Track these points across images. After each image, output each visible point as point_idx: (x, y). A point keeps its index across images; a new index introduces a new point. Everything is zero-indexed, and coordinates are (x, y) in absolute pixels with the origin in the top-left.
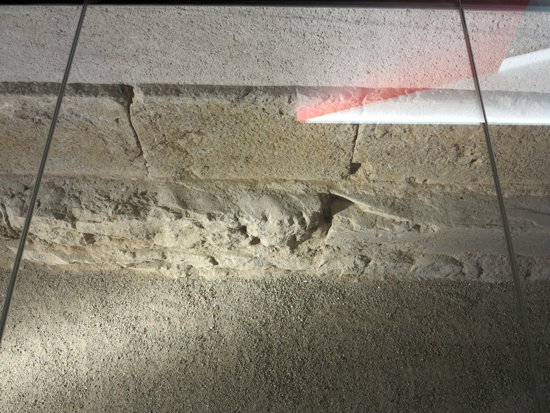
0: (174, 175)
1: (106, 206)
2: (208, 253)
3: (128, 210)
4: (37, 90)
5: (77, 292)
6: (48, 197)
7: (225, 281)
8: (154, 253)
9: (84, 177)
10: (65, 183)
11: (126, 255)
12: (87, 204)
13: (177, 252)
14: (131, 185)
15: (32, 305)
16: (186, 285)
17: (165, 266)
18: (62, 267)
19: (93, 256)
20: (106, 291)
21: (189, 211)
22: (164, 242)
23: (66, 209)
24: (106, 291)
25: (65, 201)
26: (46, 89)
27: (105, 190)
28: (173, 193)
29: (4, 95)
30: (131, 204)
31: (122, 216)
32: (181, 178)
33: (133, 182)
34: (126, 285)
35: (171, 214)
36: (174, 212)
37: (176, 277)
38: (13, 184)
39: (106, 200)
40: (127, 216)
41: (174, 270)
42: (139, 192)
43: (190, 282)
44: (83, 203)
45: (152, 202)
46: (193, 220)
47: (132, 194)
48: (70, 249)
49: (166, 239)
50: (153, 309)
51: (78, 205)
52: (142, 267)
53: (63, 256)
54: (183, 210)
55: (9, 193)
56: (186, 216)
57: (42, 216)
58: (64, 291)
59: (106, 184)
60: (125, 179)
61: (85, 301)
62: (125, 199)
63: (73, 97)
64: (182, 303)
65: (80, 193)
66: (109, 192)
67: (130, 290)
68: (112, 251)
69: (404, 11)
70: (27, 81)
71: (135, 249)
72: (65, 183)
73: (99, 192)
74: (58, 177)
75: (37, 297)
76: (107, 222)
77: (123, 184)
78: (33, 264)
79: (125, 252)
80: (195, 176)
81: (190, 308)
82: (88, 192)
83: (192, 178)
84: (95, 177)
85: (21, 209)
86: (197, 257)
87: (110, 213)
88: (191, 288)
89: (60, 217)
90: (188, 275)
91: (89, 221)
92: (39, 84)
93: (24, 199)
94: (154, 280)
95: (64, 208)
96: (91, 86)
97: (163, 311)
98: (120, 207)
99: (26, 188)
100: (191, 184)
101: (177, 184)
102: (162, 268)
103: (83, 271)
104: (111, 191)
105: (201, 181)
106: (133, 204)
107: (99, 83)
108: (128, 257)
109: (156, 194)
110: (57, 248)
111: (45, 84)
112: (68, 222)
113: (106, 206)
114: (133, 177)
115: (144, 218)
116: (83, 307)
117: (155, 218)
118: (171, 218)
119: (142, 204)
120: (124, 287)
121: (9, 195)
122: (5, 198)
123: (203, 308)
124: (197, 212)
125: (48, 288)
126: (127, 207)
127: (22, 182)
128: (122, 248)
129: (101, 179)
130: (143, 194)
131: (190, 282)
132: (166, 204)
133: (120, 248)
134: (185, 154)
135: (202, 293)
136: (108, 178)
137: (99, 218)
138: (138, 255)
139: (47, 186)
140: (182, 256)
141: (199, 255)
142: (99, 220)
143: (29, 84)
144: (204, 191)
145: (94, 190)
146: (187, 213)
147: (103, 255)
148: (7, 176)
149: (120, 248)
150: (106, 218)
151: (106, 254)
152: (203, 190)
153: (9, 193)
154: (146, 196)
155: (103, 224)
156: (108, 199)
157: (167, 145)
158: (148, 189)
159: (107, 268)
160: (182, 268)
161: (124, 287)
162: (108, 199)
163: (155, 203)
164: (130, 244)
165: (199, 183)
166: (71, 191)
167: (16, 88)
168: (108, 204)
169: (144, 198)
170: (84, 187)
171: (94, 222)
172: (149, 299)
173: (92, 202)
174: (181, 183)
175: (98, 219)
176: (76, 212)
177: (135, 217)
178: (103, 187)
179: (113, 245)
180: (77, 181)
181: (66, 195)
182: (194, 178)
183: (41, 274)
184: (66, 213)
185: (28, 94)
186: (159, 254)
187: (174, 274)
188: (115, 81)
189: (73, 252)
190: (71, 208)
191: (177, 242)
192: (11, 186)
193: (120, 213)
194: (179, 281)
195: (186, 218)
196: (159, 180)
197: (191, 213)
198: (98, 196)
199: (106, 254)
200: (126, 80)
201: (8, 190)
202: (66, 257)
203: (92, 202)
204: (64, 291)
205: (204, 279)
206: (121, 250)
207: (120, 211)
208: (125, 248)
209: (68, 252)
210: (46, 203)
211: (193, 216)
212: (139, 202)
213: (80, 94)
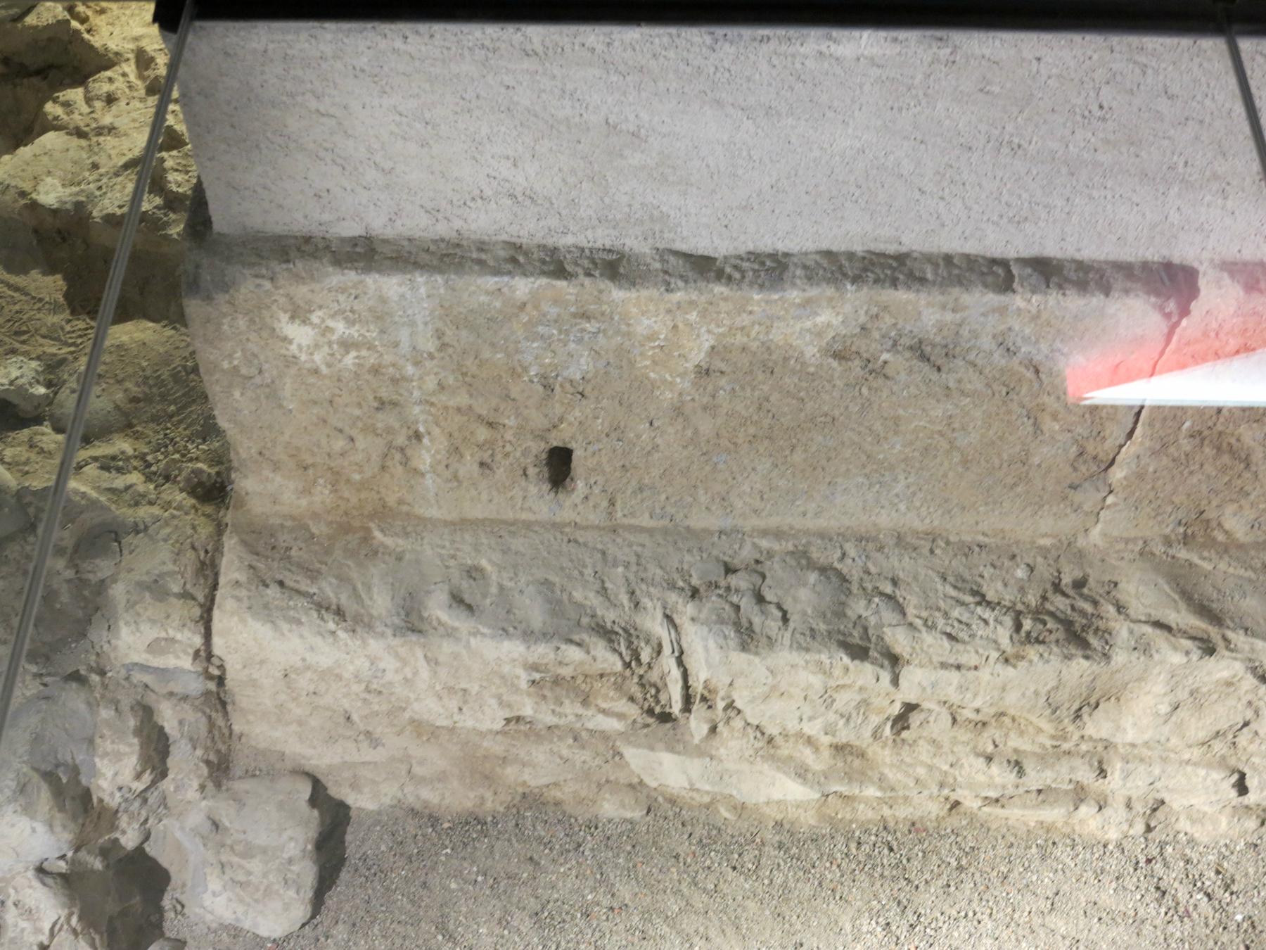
0: (1167, 531)
1: (986, 622)
2: (1233, 762)
3: (1051, 632)
4: (929, 276)
5: (820, 884)
6: (804, 594)
7: (1256, 846)
8: (1078, 762)
9: (899, 537)
10: (844, 555)
11: (995, 769)
12: (924, 614)
13: (1142, 760)
14: (1039, 559)
15: (689, 923)
16: (1142, 860)
17: (1092, 802)
18: (767, 810)
19: (891, 774)
20: (909, 881)
21: (1230, 634)
22: (1118, 728)
23: (866, 629)
24: (909, 881)
25: (858, 607)
26: (956, 272)
27: (967, 575)
28: (1168, 583)
29: (837, 289)
30: (1052, 614)
31: (1041, 648)
32: (1186, 540)
33: (1044, 552)
34: (964, 862)
35: (1187, 644)
36: (1194, 638)
37: (1113, 835)
38: (688, 558)
39: (979, 604)
40: (1055, 649)
41: (1116, 812)
42: (1067, 580)
43: (1155, 852)
44: (911, 611)
45: (1112, 610)
46: (1250, 660)
47: (1048, 586)
48: (826, 753)
49: (1136, 719)
50: (1063, 930)
51: (899, 617)
52: (1024, 806)
53: (802, 773)
54: (1214, 632)
55: (681, 584)
56: (1227, 648)
57: (807, 650)
58: (779, 881)
59: (966, 555)
60: (1017, 542)
61: (851, 912)
62: (1032, 599)
63: (1036, 299)
64: (1141, 912)
65: (895, 582)
66: (979, 580)
67: (977, 875)
68: (951, 759)
69: (882, 34)
70: (891, 249)
71: (1016, 751)
72: (844, 555)
73: (951, 579)
74: (822, 535)
75: (699, 900)
76: (999, 667)
77: (1013, 557)
78: (672, 801)
79: (989, 759)
80: (1226, 532)
81: (1171, 928)
82: (915, 578)
83: (1214, 539)
84: (933, 537)
85: (738, 631)
86: (1202, 772)
87: (1005, 642)
88: (1158, 867)
89: (859, 652)
90: (1149, 829)
91: (944, 666)
92: (929, 258)
93: (735, 599)
94: (1047, 843)
95: (859, 629)
96: (1080, 266)
97: (1092, 936)
98: (1027, 624)
99: (729, 570)
100: (1213, 555)
101: (1173, 557)
102: (1083, 809)
103: (832, 821)
104: (982, 577)
105: (1241, 547)
106: (1058, 614)
107: (1102, 258)
108: (1001, 775)
109: (1116, 584)
110: (784, 752)
111: (948, 259)
112: (882, 667)
113: (986, 622)
114: (1045, 535)
115: (1105, 655)
116: (848, 927)
117: (1136, 654)
118: (1187, 653)
119: (1083, 613)
120: (960, 868)
121: (683, 589)
122: (673, 597)
123: (1207, 925)
124: (1254, 635)
125: (731, 875)
126: (1045, 624)
127: (715, 552)
128: (980, 748)
129: (948, 543)
130: (1079, 584)
131: (1155, 852)
132: (1157, 615)
133: (975, 747)
134: (1242, 466)
135: (1195, 883)
136: (967, 538)
137: (973, 654)
138: (1029, 766)
139: (794, 563)
140: (1157, 771)
141: (1209, 766)
142: (973, 663)
143: (901, 258)
144: (1253, 576)
145: (934, 575)
146: (1225, 639)
147: (921, 771)
148: (665, 532)
149: (975, 747)
150: (995, 655)
151: (931, 768)
152: (1250, 574)
153: (681, 584)
154: (1085, 591)
155: (984, 675)
156: (983, 600)
157: (1203, 440)
158: (1089, 571)
159: (903, 812)
160: (1139, 807)
161: (960, 868)
162: (983, 600)
163: (1119, 612)
164: (1006, 735)
165: (1233, 551)
166: (865, 577)
167: (865, 270)
168: (987, 614)
169: (1086, 598)
170: (902, 564)
171: (958, 667)
172: (1044, 905)
173: (939, 609)
174: (1183, 554)
175: (969, 658)
176: (899, 640)
177: (1080, 653)
178: (958, 565)
179: (954, 741)
180: (880, 549)
181: (855, 588)
182: (1221, 538)
183: (699, 832)
184: (869, 640)
185: (909, 288)
186: (1091, 766)
187: (1104, 825)
188: (1153, 254)
189: (833, 762)
190: (880, 626)
191: (1166, 729)
192: (681, 562)
193: (1029, 639)
194: (1120, 847)
195: (1227, 653)
196: (1121, 546)
197: (1238, 638)
198: (953, 593)
199: (931, 768)
200: (1184, 252)
201: (676, 576)
202: (810, 776)
203: (939, 609)
204: (779, 881)
205: (1192, 842)
206: (978, 755)
207: (1028, 633)
208: (990, 748)
209: (817, 762)
210: (804, 614)
211: (1247, 648)
212: (1073, 608)
213: (1060, 287)
